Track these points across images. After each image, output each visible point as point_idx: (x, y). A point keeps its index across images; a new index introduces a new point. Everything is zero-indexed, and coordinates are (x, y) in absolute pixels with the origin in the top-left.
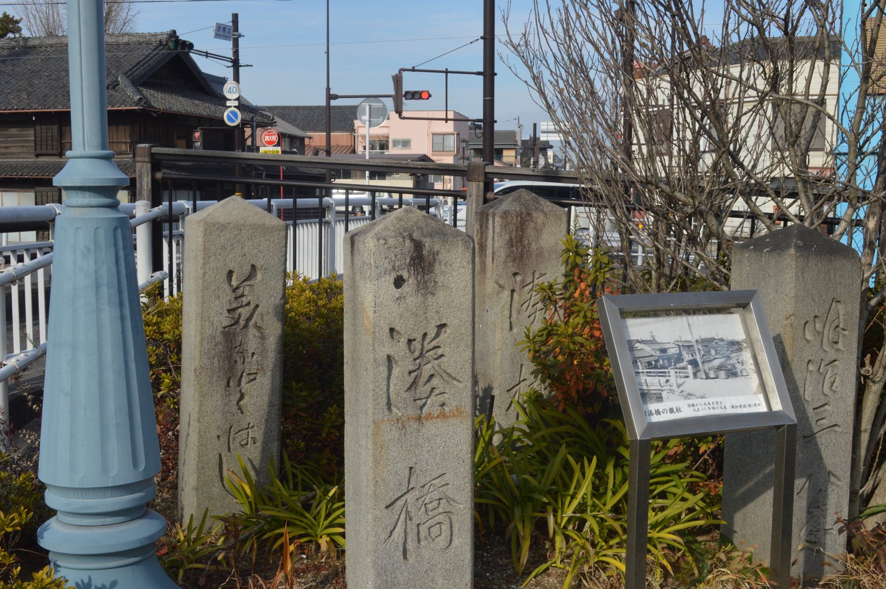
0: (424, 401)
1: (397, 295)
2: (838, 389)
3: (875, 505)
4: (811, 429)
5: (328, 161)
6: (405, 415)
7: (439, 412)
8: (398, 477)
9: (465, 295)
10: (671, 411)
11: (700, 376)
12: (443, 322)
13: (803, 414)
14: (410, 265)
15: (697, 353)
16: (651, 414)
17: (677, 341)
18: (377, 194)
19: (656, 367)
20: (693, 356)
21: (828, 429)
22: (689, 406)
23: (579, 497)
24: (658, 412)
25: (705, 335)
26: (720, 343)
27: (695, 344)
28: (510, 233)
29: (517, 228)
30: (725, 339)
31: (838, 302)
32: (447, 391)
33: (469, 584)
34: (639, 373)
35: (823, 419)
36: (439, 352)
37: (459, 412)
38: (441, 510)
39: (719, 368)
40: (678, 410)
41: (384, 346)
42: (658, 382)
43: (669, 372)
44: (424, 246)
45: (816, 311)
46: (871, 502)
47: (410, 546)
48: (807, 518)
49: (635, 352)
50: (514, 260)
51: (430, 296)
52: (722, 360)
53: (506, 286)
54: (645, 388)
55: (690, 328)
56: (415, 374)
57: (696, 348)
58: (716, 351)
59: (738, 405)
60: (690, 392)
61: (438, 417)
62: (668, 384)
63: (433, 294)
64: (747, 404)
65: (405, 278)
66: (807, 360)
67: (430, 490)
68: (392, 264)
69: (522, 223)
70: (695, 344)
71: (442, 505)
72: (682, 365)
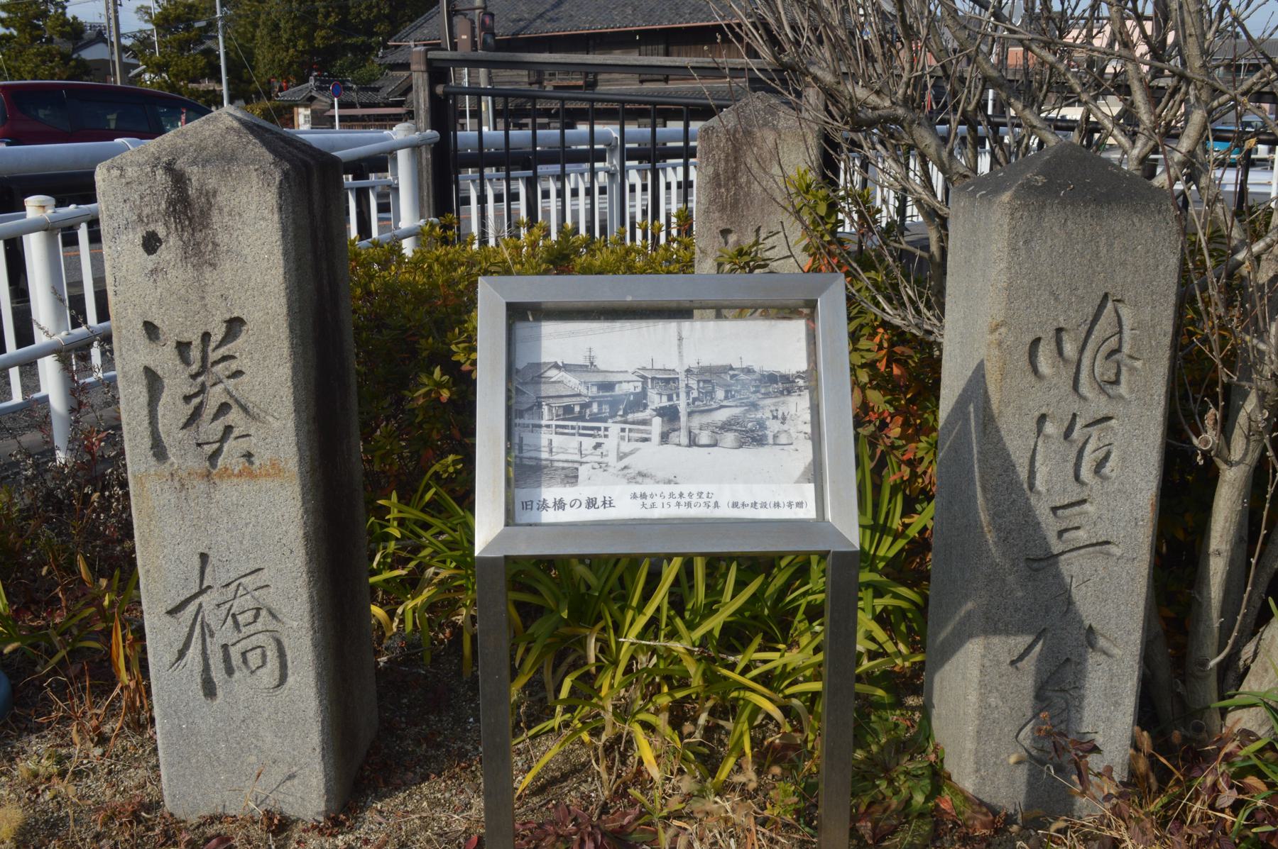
0: (216, 446)
1: (150, 266)
2: (1114, 475)
3: (1247, 690)
4: (1047, 546)
5: (677, 64)
6: (183, 467)
7: (241, 467)
8: (181, 566)
9: (271, 268)
10: (591, 503)
11: (677, 441)
12: (236, 315)
13: (1028, 516)
14: (167, 213)
15: (683, 396)
16: (543, 506)
17: (644, 369)
18: (510, 99)
19: (581, 417)
20: (670, 398)
21: (1091, 549)
22: (634, 496)
23: (650, 611)
24: (560, 505)
25: (711, 358)
26: (742, 377)
27: (682, 376)
28: (716, 164)
29: (727, 155)
30: (756, 368)
31: (1119, 301)
32: (252, 432)
33: (318, 750)
34: (540, 426)
35: (1078, 528)
36: (234, 365)
37: (275, 470)
38: (259, 626)
39: (726, 427)
40: (607, 503)
41: (137, 352)
42: (576, 445)
43: (606, 429)
44: (190, 180)
45: (1061, 319)
46: (1245, 683)
47: (218, 674)
48: (1034, 707)
49: (543, 387)
50: (723, 209)
51: (207, 269)
52: (737, 411)
53: (709, 250)
54: (544, 455)
55: (680, 346)
56: (196, 401)
57: (682, 384)
58: (727, 392)
59: (749, 501)
60: (643, 469)
61: (240, 474)
62: (599, 451)
63: (213, 266)
64: (771, 499)
65: (160, 236)
66: (1037, 414)
67: (239, 593)
68: (137, 212)
69: (736, 149)
70: (682, 376)
71: (260, 620)
72: (640, 416)
